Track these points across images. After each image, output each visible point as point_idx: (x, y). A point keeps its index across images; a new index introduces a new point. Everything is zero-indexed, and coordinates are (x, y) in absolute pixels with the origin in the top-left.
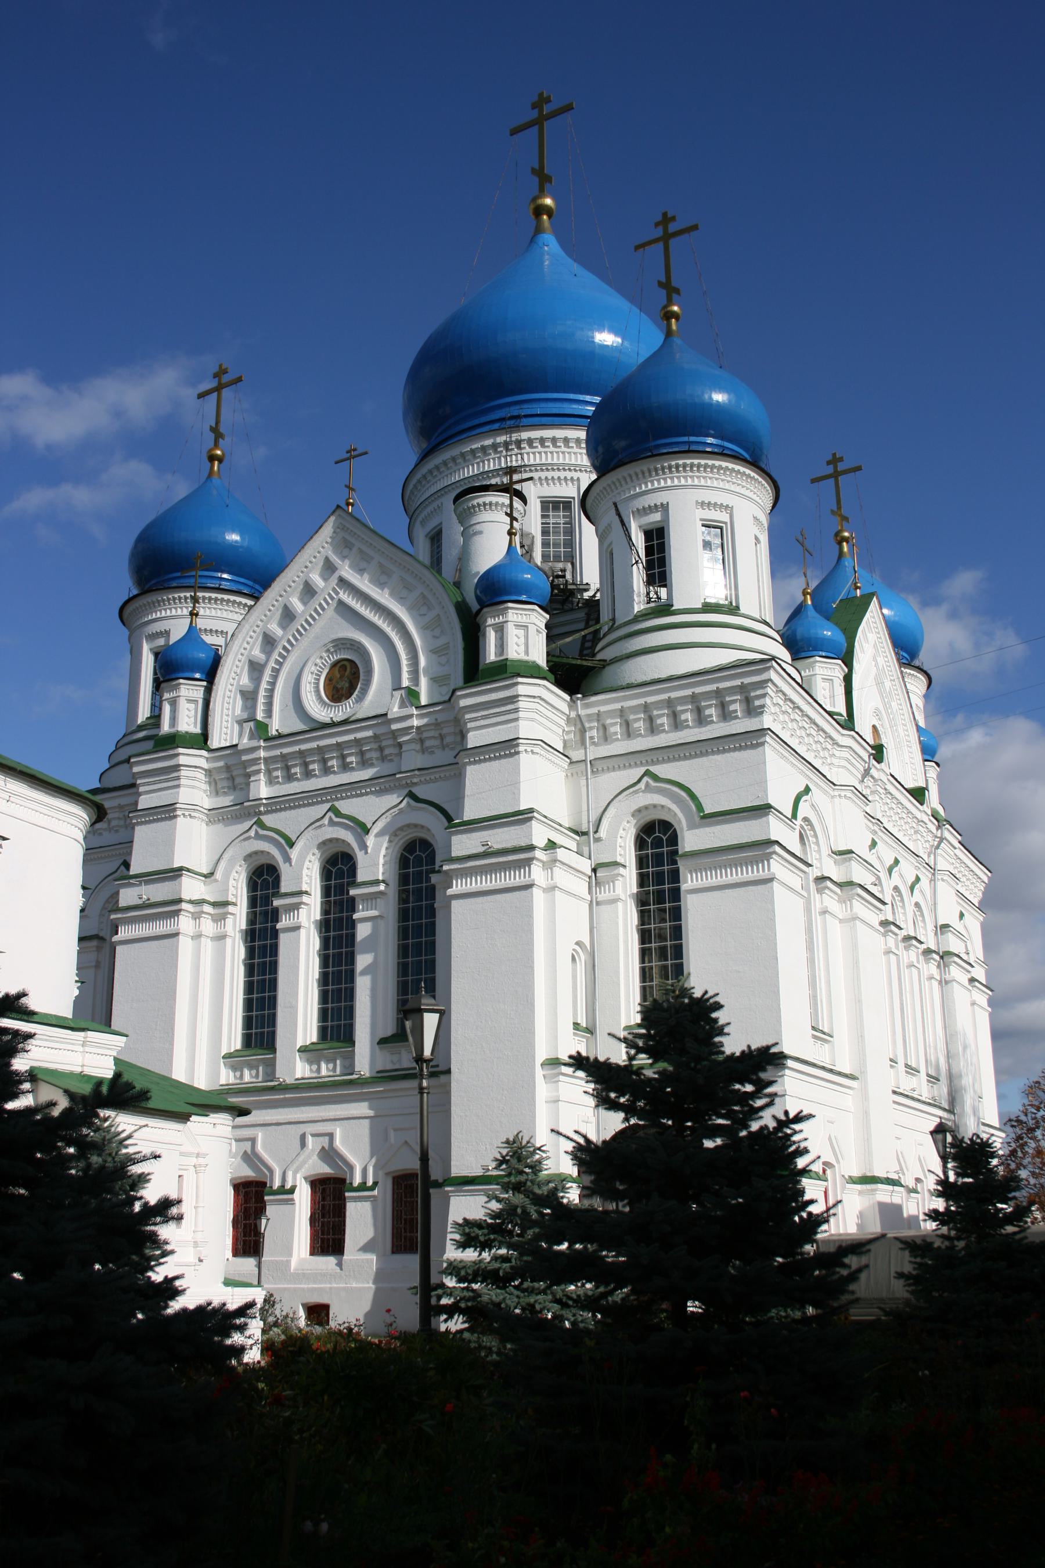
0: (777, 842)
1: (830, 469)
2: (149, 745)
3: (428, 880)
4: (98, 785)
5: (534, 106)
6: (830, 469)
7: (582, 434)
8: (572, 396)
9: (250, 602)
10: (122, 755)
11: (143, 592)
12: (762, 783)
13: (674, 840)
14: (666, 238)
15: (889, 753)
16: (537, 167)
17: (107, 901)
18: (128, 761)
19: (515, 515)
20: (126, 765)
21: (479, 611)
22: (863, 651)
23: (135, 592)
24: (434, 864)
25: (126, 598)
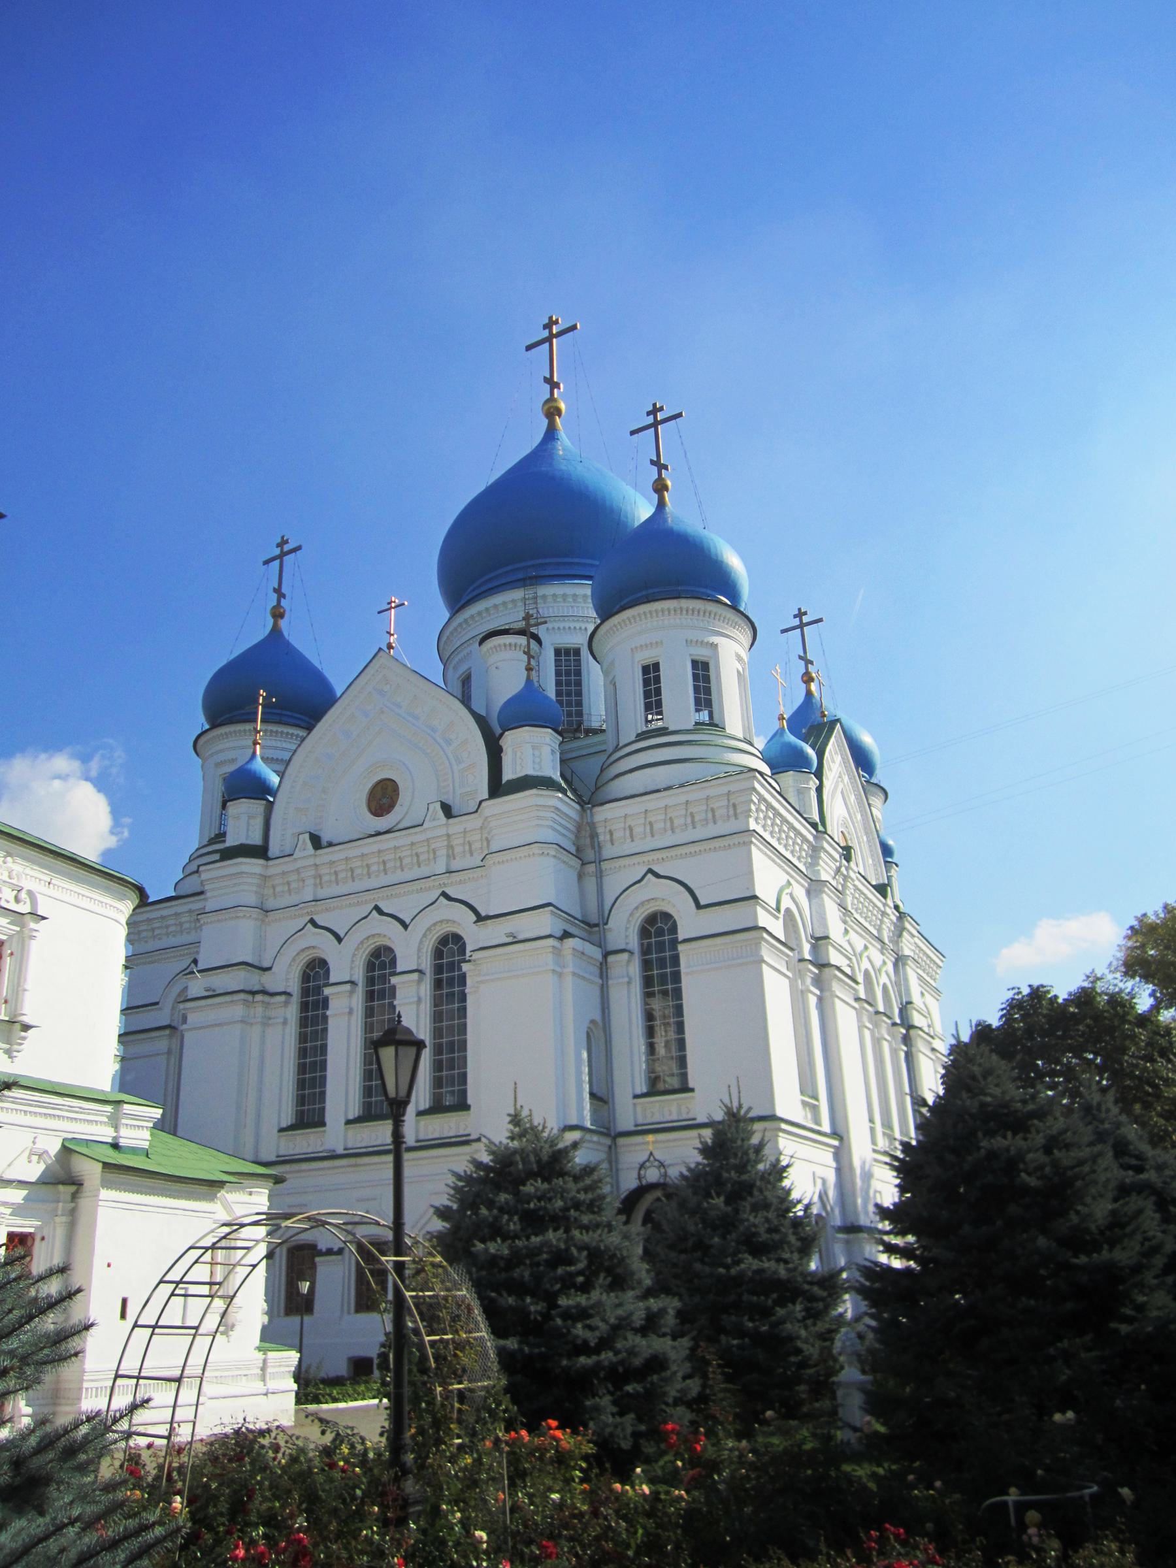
0: (764, 929)
1: (797, 622)
2: (217, 856)
3: (460, 969)
4: (174, 894)
5: (545, 327)
6: (797, 622)
7: (589, 592)
8: (576, 560)
9: (302, 733)
10: (193, 867)
11: (214, 726)
12: (748, 873)
13: (674, 929)
14: (655, 425)
15: (857, 855)
16: (548, 376)
17: (179, 995)
18: (197, 872)
19: (532, 653)
20: (195, 876)
21: (501, 735)
22: (830, 770)
23: (207, 727)
24: (464, 954)
25: (199, 732)
